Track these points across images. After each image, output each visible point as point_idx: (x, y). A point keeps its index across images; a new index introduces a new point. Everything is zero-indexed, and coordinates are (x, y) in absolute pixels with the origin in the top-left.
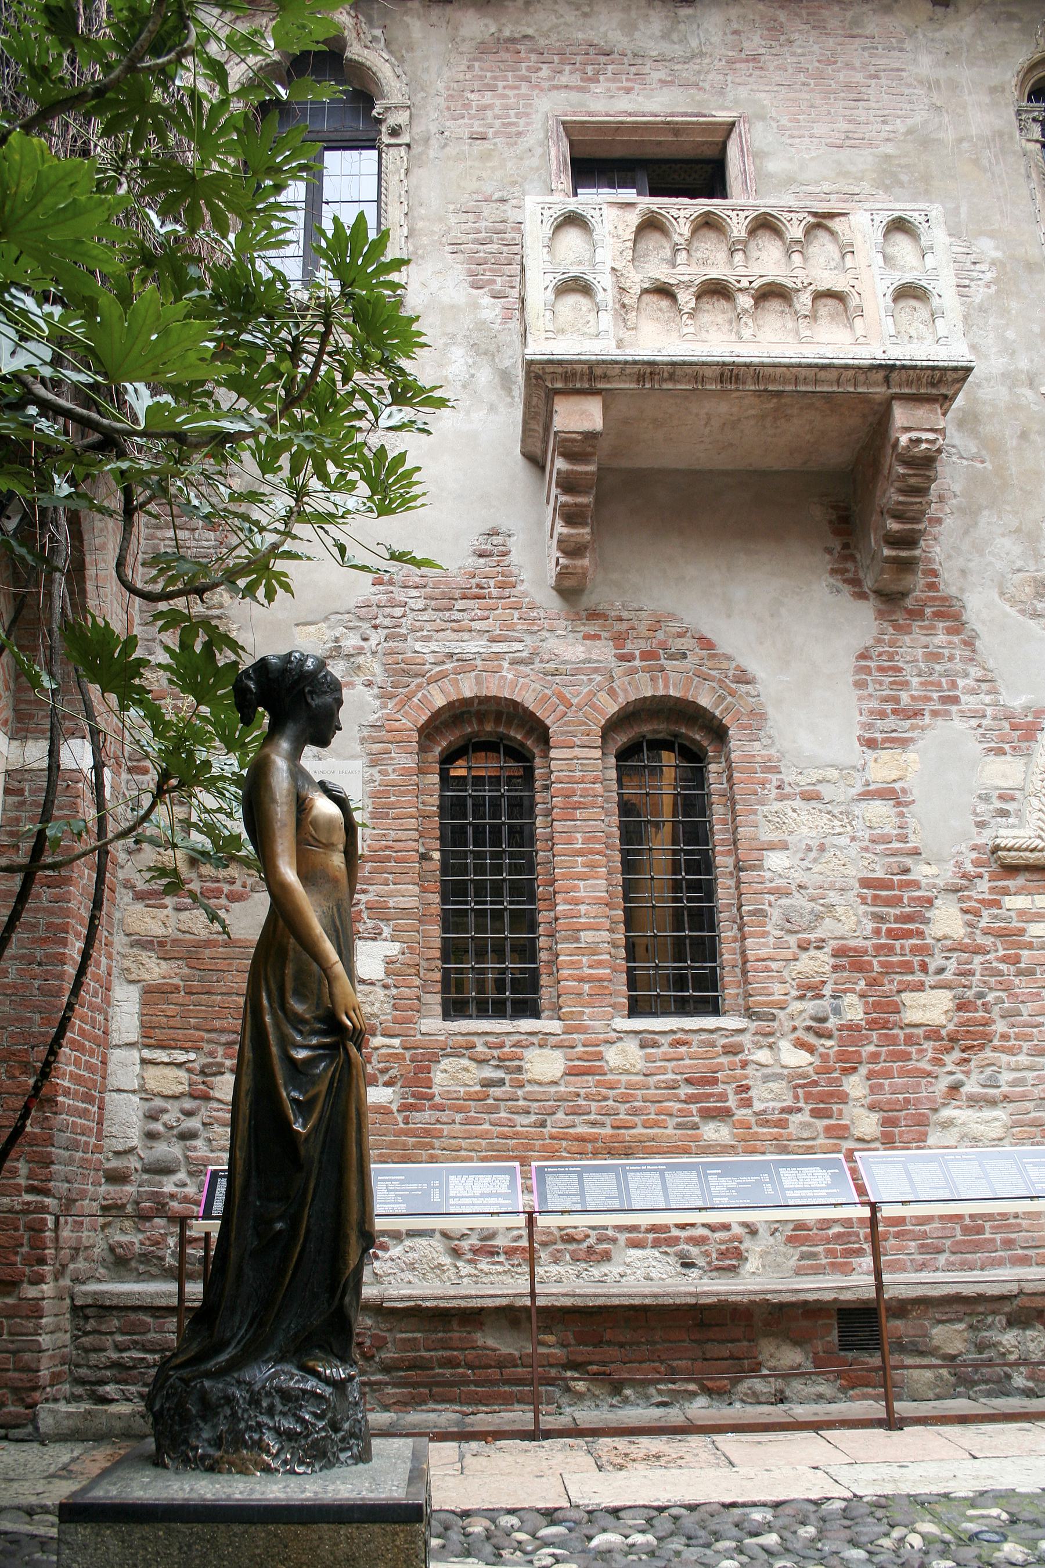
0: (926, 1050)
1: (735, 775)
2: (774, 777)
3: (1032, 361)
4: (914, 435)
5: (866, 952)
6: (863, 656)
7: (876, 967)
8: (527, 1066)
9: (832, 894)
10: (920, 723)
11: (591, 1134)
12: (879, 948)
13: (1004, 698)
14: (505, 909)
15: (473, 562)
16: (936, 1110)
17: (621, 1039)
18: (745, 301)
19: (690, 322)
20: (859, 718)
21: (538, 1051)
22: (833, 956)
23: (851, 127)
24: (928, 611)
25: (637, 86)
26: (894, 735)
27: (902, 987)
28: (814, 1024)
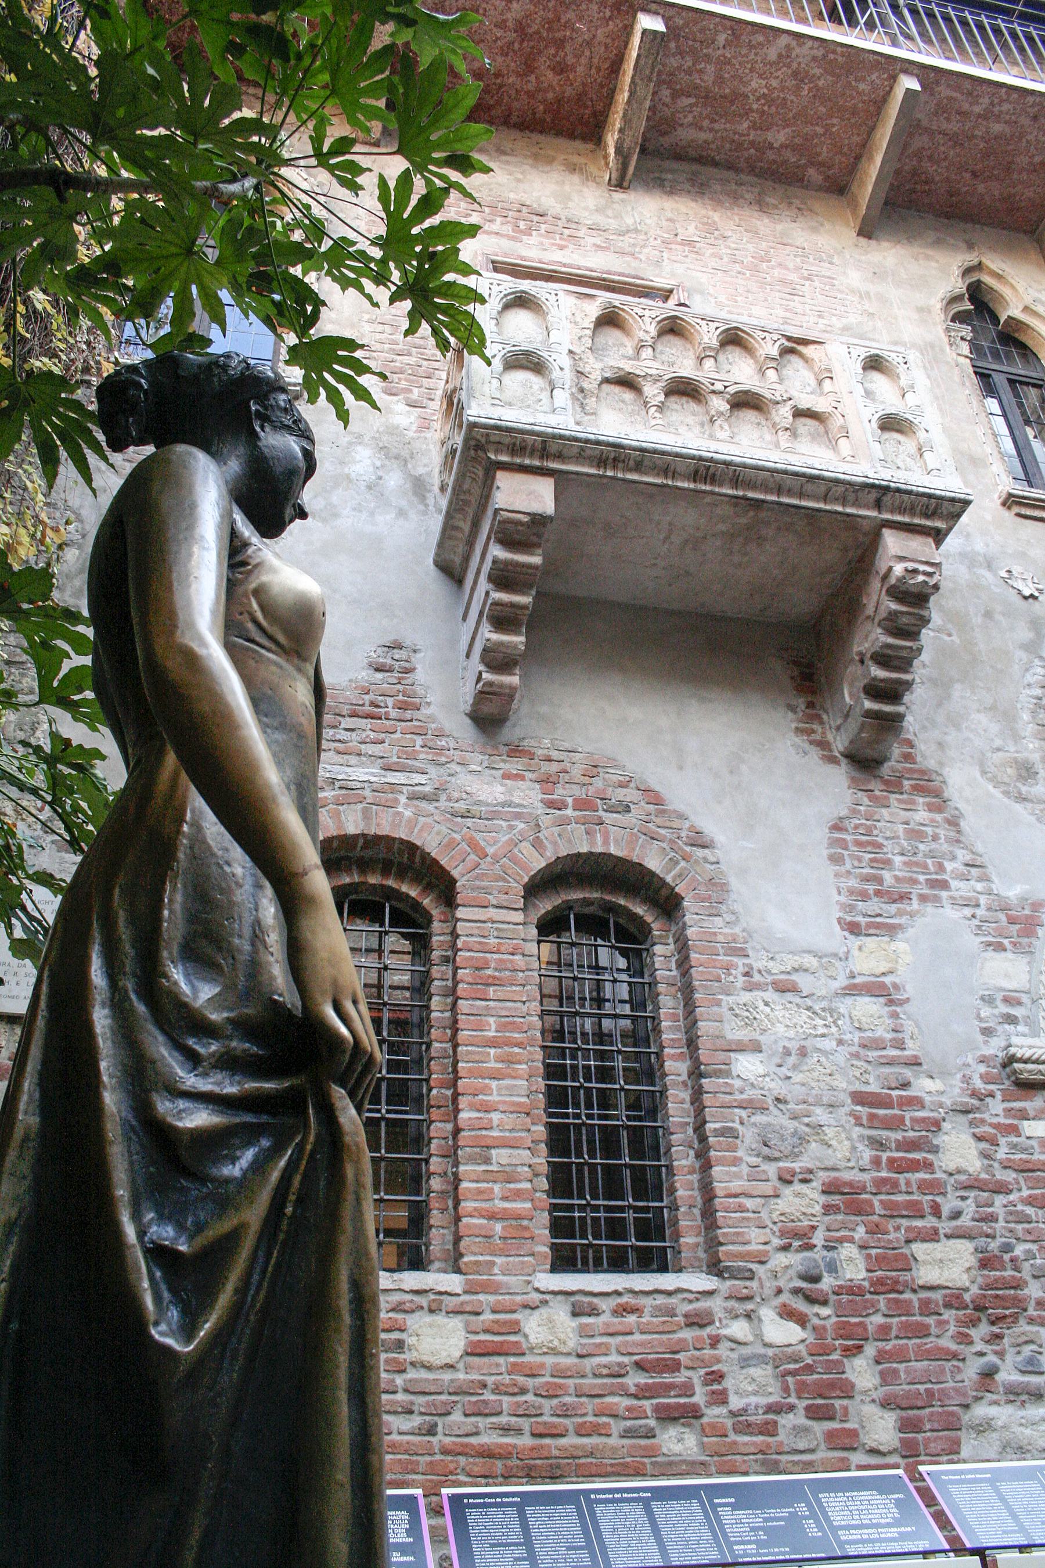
0: (947, 1322)
1: (693, 955)
2: (740, 962)
3: (987, 545)
4: (911, 566)
5: (863, 1189)
6: (836, 827)
7: (878, 1208)
8: (411, 1341)
9: (818, 1110)
10: (908, 909)
11: (501, 1446)
12: (880, 1183)
13: (997, 886)
14: (383, 1118)
15: (366, 675)
16: (967, 1407)
17: (545, 1302)
18: (719, 404)
19: (657, 415)
20: (837, 898)
21: (428, 1319)
22: (824, 1192)
23: (788, 315)
24: (906, 783)
25: (571, 246)
26: (878, 920)
27: (911, 1236)
28: (804, 1285)
